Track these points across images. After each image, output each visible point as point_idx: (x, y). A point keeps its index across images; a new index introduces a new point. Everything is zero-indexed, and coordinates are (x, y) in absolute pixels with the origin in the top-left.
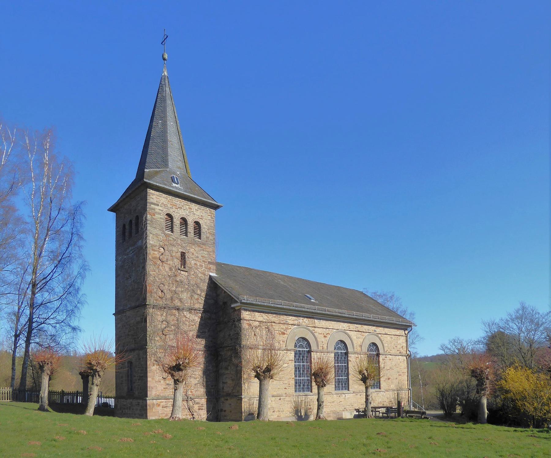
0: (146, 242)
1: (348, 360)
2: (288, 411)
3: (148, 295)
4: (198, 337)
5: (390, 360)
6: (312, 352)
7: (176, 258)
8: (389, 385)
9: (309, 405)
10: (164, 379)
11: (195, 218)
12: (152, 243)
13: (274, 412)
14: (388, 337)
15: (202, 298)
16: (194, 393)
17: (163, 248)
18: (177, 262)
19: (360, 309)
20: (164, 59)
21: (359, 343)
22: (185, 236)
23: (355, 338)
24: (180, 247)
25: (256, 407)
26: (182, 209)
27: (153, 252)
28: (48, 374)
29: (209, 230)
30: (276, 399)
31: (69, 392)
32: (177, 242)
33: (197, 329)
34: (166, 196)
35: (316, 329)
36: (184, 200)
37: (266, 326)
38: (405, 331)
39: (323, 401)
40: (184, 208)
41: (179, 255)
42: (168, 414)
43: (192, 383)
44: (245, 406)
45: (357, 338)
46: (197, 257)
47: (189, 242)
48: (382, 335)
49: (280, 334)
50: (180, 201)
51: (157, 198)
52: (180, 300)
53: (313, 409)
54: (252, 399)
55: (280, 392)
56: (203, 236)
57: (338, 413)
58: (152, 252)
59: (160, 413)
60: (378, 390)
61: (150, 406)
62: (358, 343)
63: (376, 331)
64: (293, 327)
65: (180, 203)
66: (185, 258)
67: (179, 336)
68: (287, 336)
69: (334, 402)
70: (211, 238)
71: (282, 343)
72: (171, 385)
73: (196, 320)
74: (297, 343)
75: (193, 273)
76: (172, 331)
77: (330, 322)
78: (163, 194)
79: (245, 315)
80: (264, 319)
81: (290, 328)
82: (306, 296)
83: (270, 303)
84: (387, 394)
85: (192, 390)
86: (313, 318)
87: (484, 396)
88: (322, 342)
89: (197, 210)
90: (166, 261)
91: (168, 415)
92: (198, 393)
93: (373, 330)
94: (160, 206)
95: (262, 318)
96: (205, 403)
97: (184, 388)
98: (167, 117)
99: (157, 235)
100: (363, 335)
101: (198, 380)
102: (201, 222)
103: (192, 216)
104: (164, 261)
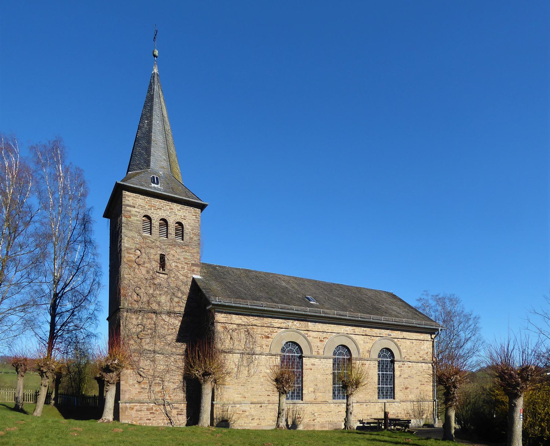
0: (121, 245)
1: (352, 367)
2: (270, 419)
3: (122, 298)
4: (178, 340)
5: (409, 367)
6: (304, 357)
7: (155, 261)
8: (407, 396)
9: (298, 414)
10: (139, 382)
11: (177, 219)
12: (127, 245)
14: (407, 342)
15: (184, 301)
16: (172, 398)
17: (140, 251)
18: (155, 265)
19: (376, 310)
20: (155, 56)
21: (367, 348)
22: (166, 237)
23: (362, 342)
24: (159, 249)
25: (231, 414)
28: (22, 376)
29: (193, 230)
30: (255, 406)
31: (91, 396)
32: (156, 244)
33: (177, 333)
34: (144, 197)
35: (310, 333)
36: (164, 201)
37: (246, 329)
38: (431, 335)
39: (283, 408)
40: (165, 209)
42: (143, 418)
43: (171, 388)
44: (218, 412)
45: (364, 343)
46: (179, 259)
47: (170, 243)
49: (263, 338)
51: (133, 200)
52: (159, 303)
53: (303, 418)
55: (261, 399)
57: (336, 423)
58: (127, 255)
59: (134, 416)
60: (392, 400)
61: (122, 410)
62: (365, 348)
63: (391, 335)
64: (280, 330)
65: (159, 204)
66: (164, 260)
68: (272, 340)
69: (331, 411)
70: (195, 238)
71: (265, 348)
72: (146, 389)
73: (176, 324)
74: (285, 347)
75: (173, 275)
76: (148, 335)
77: (328, 325)
78: (140, 196)
79: (220, 317)
80: (243, 322)
81: (276, 332)
82: (306, 297)
83: (249, 304)
84: (403, 405)
85: (171, 395)
86: (306, 321)
87: (451, 407)
88: (318, 347)
89: (180, 210)
90: (143, 264)
91: (143, 419)
93: (386, 334)
94: (137, 208)
95: (241, 320)
96: (185, 408)
97: (162, 392)
98: (152, 116)
99: (133, 238)
100: (373, 340)
101: (177, 384)
102: (183, 222)
104: (140, 263)
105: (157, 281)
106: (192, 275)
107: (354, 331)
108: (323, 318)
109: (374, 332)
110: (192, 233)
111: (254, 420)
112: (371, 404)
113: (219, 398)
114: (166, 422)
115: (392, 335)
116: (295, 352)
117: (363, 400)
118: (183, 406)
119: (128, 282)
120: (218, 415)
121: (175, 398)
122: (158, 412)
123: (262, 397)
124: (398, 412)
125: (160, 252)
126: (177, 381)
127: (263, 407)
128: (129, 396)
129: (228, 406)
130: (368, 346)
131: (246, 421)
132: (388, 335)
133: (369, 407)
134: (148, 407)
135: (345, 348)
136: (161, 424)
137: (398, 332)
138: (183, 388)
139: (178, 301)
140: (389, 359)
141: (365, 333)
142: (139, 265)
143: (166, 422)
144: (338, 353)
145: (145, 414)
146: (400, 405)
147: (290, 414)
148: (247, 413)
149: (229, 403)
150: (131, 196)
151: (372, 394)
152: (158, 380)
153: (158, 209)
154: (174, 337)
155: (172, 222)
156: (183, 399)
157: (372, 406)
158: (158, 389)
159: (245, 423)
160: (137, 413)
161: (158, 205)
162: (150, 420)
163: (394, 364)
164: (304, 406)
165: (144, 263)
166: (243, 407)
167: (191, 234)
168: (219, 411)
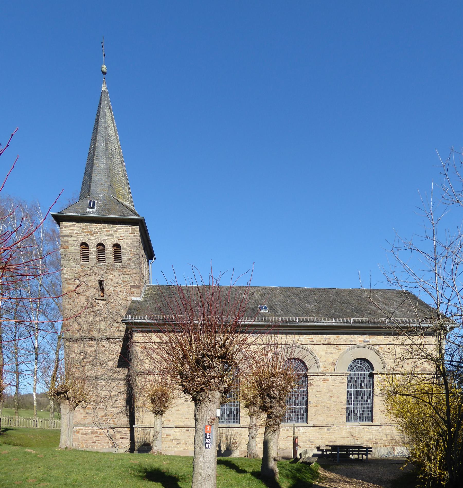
4: (119, 366)
6: (376, 374)
7: (93, 288)
9: (233, 439)
11: (114, 241)
13: (178, 444)
18: (93, 292)
19: (358, 310)
21: (331, 360)
23: (323, 353)
26: (98, 234)
27: (68, 286)
30: (181, 429)
34: (80, 224)
36: (100, 224)
41: (97, 284)
44: (139, 435)
45: (326, 353)
46: (118, 283)
48: (381, 346)
50: (96, 225)
51: (70, 229)
53: (240, 444)
54: (148, 428)
56: (124, 259)
57: (283, 450)
58: (67, 286)
59: (80, 439)
65: (95, 229)
67: (97, 367)
76: (90, 362)
78: (77, 224)
85: (115, 420)
89: (116, 231)
92: (120, 422)
93: (361, 341)
96: (129, 432)
100: (340, 349)
101: (120, 409)
103: (110, 239)
105: (96, 309)
106: (131, 298)
107: (311, 340)
108: (298, 328)
109: (342, 339)
110: (130, 253)
111: (180, 444)
112: (335, 428)
113: (140, 422)
114: (110, 445)
115: (371, 342)
116: (365, 370)
117: (324, 423)
118: (126, 430)
119: (69, 312)
120: (139, 438)
121: (119, 422)
122: (102, 436)
123: (190, 420)
124: (377, 437)
125: (98, 279)
126: (119, 405)
127: (190, 431)
128: (75, 421)
129: (150, 430)
130: (332, 358)
131: (171, 446)
132: (364, 342)
133: (332, 431)
134: (93, 431)
135: (365, 362)
136: (106, 447)
137: (381, 336)
138: (126, 412)
139: (118, 327)
140: (366, 373)
141: (329, 341)
142: (78, 294)
143: (110, 445)
144: (356, 368)
145: (90, 437)
146: (380, 429)
147: (224, 438)
148: (172, 437)
149: (151, 426)
150: (67, 226)
151: (337, 416)
152: (101, 405)
153: (95, 233)
154: (115, 362)
155: (109, 246)
156: (126, 424)
157: (337, 430)
158: (101, 414)
159: (169, 447)
160: (83, 436)
161: (94, 230)
162: (95, 443)
163: (373, 378)
164: (241, 430)
165: (83, 291)
166: (167, 431)
167: (129, 255)
168: (140, 435)
